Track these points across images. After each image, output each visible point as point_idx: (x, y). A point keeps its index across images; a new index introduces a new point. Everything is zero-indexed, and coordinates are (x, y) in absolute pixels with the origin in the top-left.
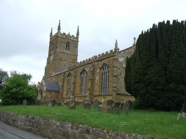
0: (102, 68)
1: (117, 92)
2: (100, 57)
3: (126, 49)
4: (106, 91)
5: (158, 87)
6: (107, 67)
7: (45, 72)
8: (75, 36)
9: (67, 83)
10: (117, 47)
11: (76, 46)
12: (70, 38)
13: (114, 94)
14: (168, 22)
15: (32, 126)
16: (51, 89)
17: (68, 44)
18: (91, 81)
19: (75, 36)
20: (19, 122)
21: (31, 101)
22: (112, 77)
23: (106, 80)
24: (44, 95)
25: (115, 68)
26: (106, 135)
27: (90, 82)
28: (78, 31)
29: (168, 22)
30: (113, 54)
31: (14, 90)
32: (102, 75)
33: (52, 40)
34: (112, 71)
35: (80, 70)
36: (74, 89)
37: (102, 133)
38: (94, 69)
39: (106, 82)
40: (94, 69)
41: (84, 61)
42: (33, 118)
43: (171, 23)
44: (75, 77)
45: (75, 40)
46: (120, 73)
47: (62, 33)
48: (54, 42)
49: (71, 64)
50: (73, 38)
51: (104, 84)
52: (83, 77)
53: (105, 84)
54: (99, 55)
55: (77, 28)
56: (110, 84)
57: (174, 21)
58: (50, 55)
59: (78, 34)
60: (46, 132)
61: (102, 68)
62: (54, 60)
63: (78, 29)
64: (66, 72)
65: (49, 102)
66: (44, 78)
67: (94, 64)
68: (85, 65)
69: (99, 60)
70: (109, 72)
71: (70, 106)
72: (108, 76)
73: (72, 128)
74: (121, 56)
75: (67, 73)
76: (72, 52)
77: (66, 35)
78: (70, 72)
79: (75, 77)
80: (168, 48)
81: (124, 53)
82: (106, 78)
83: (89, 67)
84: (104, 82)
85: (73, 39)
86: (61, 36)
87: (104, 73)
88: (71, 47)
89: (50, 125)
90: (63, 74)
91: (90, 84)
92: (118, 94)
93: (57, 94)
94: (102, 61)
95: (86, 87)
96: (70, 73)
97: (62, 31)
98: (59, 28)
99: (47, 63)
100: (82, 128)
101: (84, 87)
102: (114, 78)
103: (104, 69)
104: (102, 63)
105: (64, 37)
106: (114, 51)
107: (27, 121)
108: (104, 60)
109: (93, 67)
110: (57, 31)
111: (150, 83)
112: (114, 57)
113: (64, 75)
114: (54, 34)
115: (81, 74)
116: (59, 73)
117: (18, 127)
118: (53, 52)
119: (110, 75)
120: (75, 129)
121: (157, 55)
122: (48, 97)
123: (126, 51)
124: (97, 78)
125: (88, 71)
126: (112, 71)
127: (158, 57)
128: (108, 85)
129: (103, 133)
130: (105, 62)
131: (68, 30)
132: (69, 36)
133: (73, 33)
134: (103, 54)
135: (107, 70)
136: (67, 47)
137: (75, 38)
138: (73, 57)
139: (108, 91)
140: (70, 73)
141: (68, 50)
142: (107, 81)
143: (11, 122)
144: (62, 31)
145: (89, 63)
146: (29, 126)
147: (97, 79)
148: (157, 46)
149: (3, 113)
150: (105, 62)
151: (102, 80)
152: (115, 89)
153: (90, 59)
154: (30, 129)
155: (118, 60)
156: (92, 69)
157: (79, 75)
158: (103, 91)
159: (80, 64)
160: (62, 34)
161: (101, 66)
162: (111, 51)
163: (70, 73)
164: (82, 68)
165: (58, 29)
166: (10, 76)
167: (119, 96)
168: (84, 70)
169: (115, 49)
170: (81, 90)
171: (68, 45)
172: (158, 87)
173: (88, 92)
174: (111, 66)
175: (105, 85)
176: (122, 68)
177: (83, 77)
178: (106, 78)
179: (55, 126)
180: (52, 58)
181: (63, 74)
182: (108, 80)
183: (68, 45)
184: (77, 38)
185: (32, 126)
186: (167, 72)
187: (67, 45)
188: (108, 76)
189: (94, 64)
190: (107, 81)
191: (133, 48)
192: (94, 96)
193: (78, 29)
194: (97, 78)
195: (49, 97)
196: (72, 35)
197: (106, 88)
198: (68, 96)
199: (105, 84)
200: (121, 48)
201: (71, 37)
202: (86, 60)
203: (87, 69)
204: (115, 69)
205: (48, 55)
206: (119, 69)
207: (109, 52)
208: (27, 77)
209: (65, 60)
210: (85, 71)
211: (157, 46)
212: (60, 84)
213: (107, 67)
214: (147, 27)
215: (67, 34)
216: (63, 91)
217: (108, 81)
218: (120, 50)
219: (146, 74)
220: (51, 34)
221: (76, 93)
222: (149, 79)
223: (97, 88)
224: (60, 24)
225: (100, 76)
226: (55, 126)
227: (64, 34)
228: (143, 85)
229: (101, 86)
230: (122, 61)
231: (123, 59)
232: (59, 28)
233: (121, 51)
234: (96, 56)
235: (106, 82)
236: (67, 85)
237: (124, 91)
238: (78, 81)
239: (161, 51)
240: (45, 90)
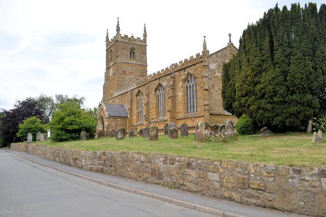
0: (186, 80)
1: (211, 112)
2: (181, 64)
3: (219, 51)
4: (194, 112)
5: (275, 99)
6: (193, 78)
7: (104, 92)
8: (142, 38)
9: (137, 104)
10: (206, 49)
11: (144, 53)
12: (134, 42)
13: (207, 114)
14: (285, 8)
15: (104, 164)
16: (116, 114)
17: (132, 50)
18: (171, 99)
19: (142, 38)
20: (83, 161)
21: (91, 133)
22: (201, 91)
23: (193, 97)
24: (106, 123)
25: (205, 78)
26: (218, 169)
27: (170, 100)
28: (145, 31)
29: (285, 8)
30: (202, 59)
31: (67, 119)
32: (187, 89)
33: (109, 47)
34: (201, 83)
35: (154, 85)
36: (148, 112)
37: (212, 167)
38: (174, 82)
39: (193, 98)
40: (174, 82)
41: (159, 72)
42: (104, 154)
43: (289, 8)
44: (148, 95)
45: (143, 44)
46: (213, 86)
47: (123, 35)
48: (112, 49)
49: (138, 78)
51: (190, 102)
53: (192, 102)
54: (181, 62)
56: (198, 101)
57: (294, 6)
58: (108, 68)
59: (145, 36)
60: (125, 171)
61: (186, 80)
62: (114, 74)
63: (145, 28)
65: (117, 132)
66: (104, 100)
67: (174, 75)
69: (181, 70)
70: (196, 85)
71: (151, 135)
72: (196, 91)
73: (165, 162)
75: (135, 91)
76: (139, 61)
77: (129, 38)
79: (148, 95)
80: (287, 45)
81: (216, 57)
82: (193, 94)
83: (167, 80)
84: (190, 99)
85: (139, 43)
86: (122, 40)
87: (190, 86)
88: (137, 53)
89: (131, 161)
90: (129, 93)
91: (170, 104)
92: (211, 114)
93: (124, 121)
94: (184, 71)
95: (165, 109)
96: (139, 91)
97: (123, 33)
98: (118, 30)
99: (105, 80)
100: (180, 162)
101: (161, 108)
102: (205, 92)
103: (188, 81)
104: (186, 73)
105: (127, 41)
106: (201, 54)
107: (95, 158)
108: (188, 69)
109: (172, 79)
110: (115, 33)
111: (264, 94)
112: (204, 64)
114: (111, 37)
115: (156, 90)
116: (125, 91)
117: (83, 167)
118: (112, 64)
120: (170, 164)
121: (272, 54)
123: (219, 54)
124: (180, 94)
126: (201, 83)
127: (274, 57)
128: (197, 104)
129: (213, 166)
131: (132, 30)
132: (132, 38)
133: (139, 35)
134: (186, 60)
136: (131, 54)
137: (141, 41)
138: (141, 68)
139: (197, 111)
140: (139, 91)
141: (134, 58)
142: (195, 97)
143: (72, 162)
144: (123, 33)
145: (167, 74)
146: (98, 165)
147: (180, 96)
148: (271, 42)
149: (58, 150)
150: (190, 71)
151: (187, 96)
152: (207, 108)
153: (167, 69)
154: (102, 169)
155: (209, 67)
156: (171, 83)
158: (189, 112)
159: (152, 77)
160: (122, 37)
161: (184, 77)
162: (198, 55)
164: (157, 82)
165: (117, 30)
166: (55, 101)
167: (213, 116)
168: (160, 85)
169: (204, 52)
170: (158, 113)
171: (132, 52)
172: (275, 99)
173: (169, 114)
174: (198, 76)
175: (192, 103)
176: (215, 77)
178: (193, 94)
179: (138, 162)
180: (111, 71)
181: (129, 93)
182: (196, 96)
183: (132, 52)
184: (145, 40)
185: (104, 164)
186: (288, 78)
187: (131, 52)
188: (195, 90)
189: (174, 75)
190: (195, 97)
191: (228, 48)
192: (177, 120)
193: (145, 28)
194: (180, 94)
195: (114, 125)
197: (194, 107)
198: (140, 122)
199: (192, 102)
200: (212, 50)
201: (135, 40)
202: (162, 70)
204: (205, 80)
205: (105, 68)
206: (211, 79)
207: (195, 57)
208: (77, 102)
209: (131, 73)
210: (162, 86)
211: (271, 42)
212: (127, 107)
213: (193, 78)
214: (255, 16)
215: (129, 36)
216: (131, 116)
217: (196, 98)
218: (210, 53)
219: (258, 83)
220: (107, 38)
221: (151, 117)
222: (262, 89)
223: (180, 108)
225: (184, 91)
226: (138, 162)
227: (126, 36)
228: (253, 97)
229: (186, 104)
230: (214, 68)
231: (216, 65)
232: (118, 30)
233: (212, 55)
234: (176, 64)
235: (193, 98)
236: (138, 108)
237: (220, 109)
238: (153, 100)
239: (277, 49)
240: (107, 116)
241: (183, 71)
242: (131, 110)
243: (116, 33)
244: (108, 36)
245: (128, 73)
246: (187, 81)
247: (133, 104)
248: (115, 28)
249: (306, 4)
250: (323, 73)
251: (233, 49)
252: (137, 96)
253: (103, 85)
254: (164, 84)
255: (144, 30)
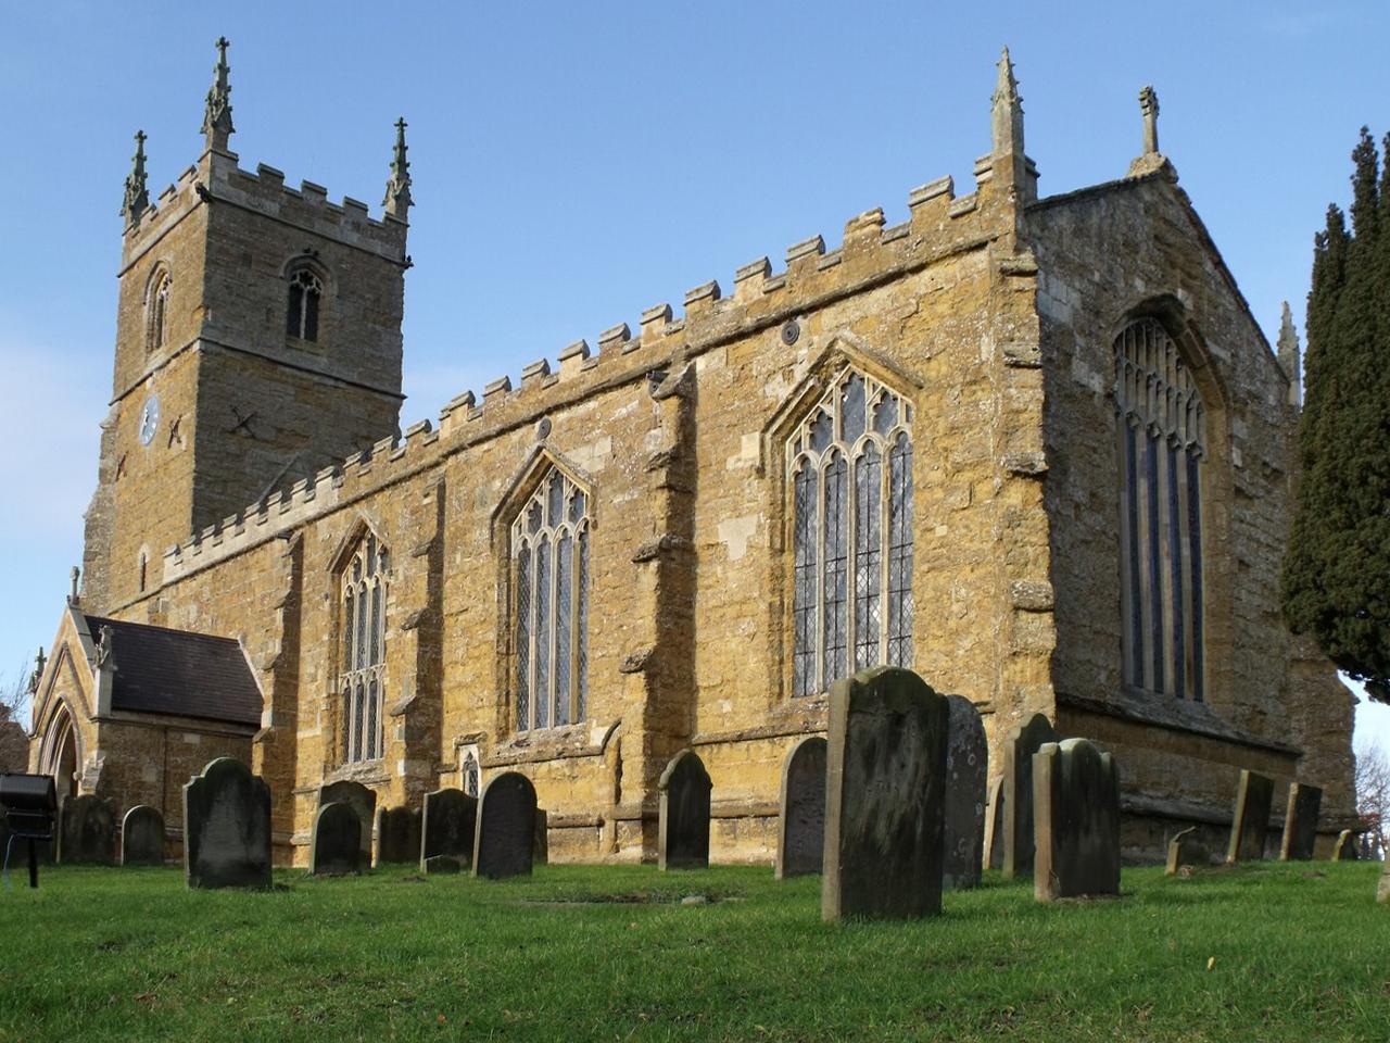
12: (320, 226)
19: (377, 214)
45: (378, 248)
47: (249, 165)
50: (357, 227)
52: (350, 600)
55: (395, 142)
64: (311, 521)
68: (558, 408)
74: (1058, 255)
77: (292, 194)
78: (362, 511)
85: (354, 238)
94: (791, 337)
96: (361, 533)
98: (222, 125)
104: (805, 355)
105: (272, 208)
108: (828, 316)
113: (297, 552)
115: (506, 512)
119: (936, 476)
122: (142, 784)
125: (608, 476)
130: (848, 334)
132: (313, 199)
135: (553, 536)
141: (312, 335)
145: (615, 375)
157: (481, 535)
163: (363, 528)
168: (544, 471)
174: (937, 370)
177: (350, 600)
184: (396, 227)
195: (150, 776)
196: (349, 202)
201: (332, 213)
203: (584, 451)
215: (293, 182)
224: (147, 167)
225: (778, 508)
227: (271, 177)
232: (222, 125)
233: (1054, 202)
236: (340, 660)
241: (775, 336)
242: (286, 669)
243: (202, 144)
244: (140, 173)
245: (270, 435)
246: (804, 429)
247: (305, 629)
248: (199, 111)
249: (1333, 208)
250: (670, 979)
251: (1173, 212)
252: (339, 568)
253: (85, 509)
254: (586, 458)
255: (393, 156)
